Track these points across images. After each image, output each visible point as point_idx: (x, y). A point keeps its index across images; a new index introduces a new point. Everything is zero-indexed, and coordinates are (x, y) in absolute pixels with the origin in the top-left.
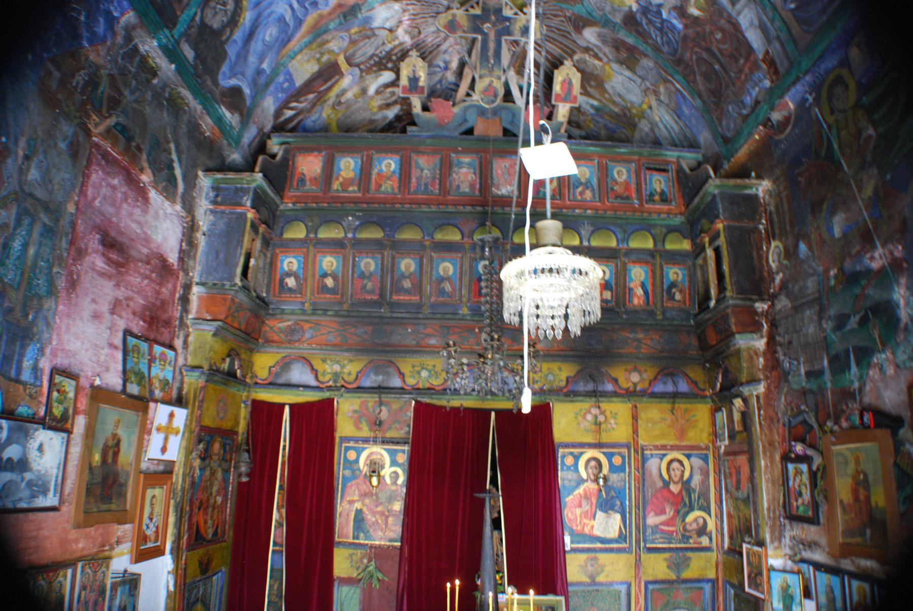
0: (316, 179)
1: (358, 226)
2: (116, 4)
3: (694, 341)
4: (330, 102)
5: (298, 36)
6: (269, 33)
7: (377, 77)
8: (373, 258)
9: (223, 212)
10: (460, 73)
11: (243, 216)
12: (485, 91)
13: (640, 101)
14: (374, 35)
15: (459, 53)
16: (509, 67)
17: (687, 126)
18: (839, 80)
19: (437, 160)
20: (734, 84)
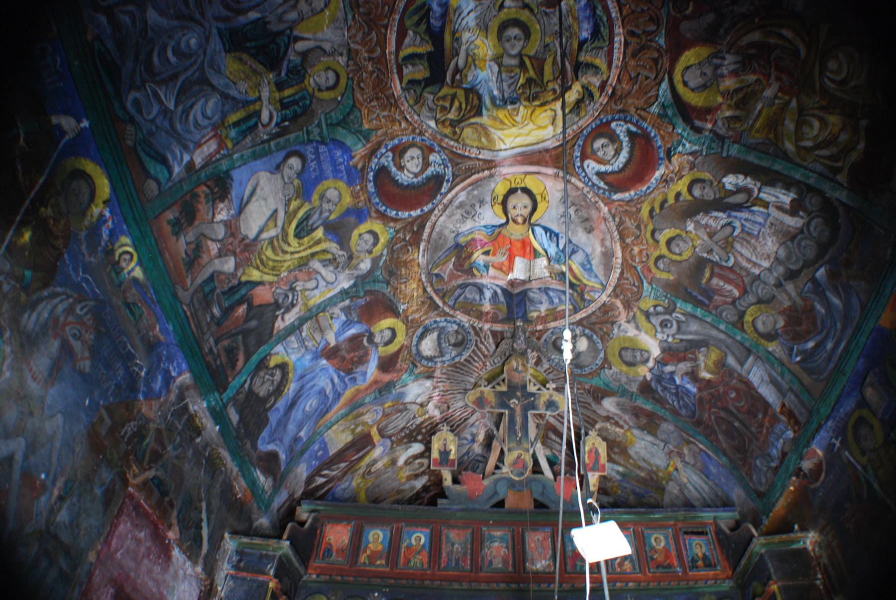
0: (343, 550)
2: (175, 364)
4: (361, 471)
5: (336, 408)
6: (310, 404)
7: (407, 449)
9: (244, 579)
10: (488, 444)
11: (264, 585)
12: (514, 464)
13: (665, 465)
14: (406, 409)
15: (486, 426)
16: (536, 439)
17: (717, 485)
18: (861, 420)
19: (468, 533)
20: (757, 439)
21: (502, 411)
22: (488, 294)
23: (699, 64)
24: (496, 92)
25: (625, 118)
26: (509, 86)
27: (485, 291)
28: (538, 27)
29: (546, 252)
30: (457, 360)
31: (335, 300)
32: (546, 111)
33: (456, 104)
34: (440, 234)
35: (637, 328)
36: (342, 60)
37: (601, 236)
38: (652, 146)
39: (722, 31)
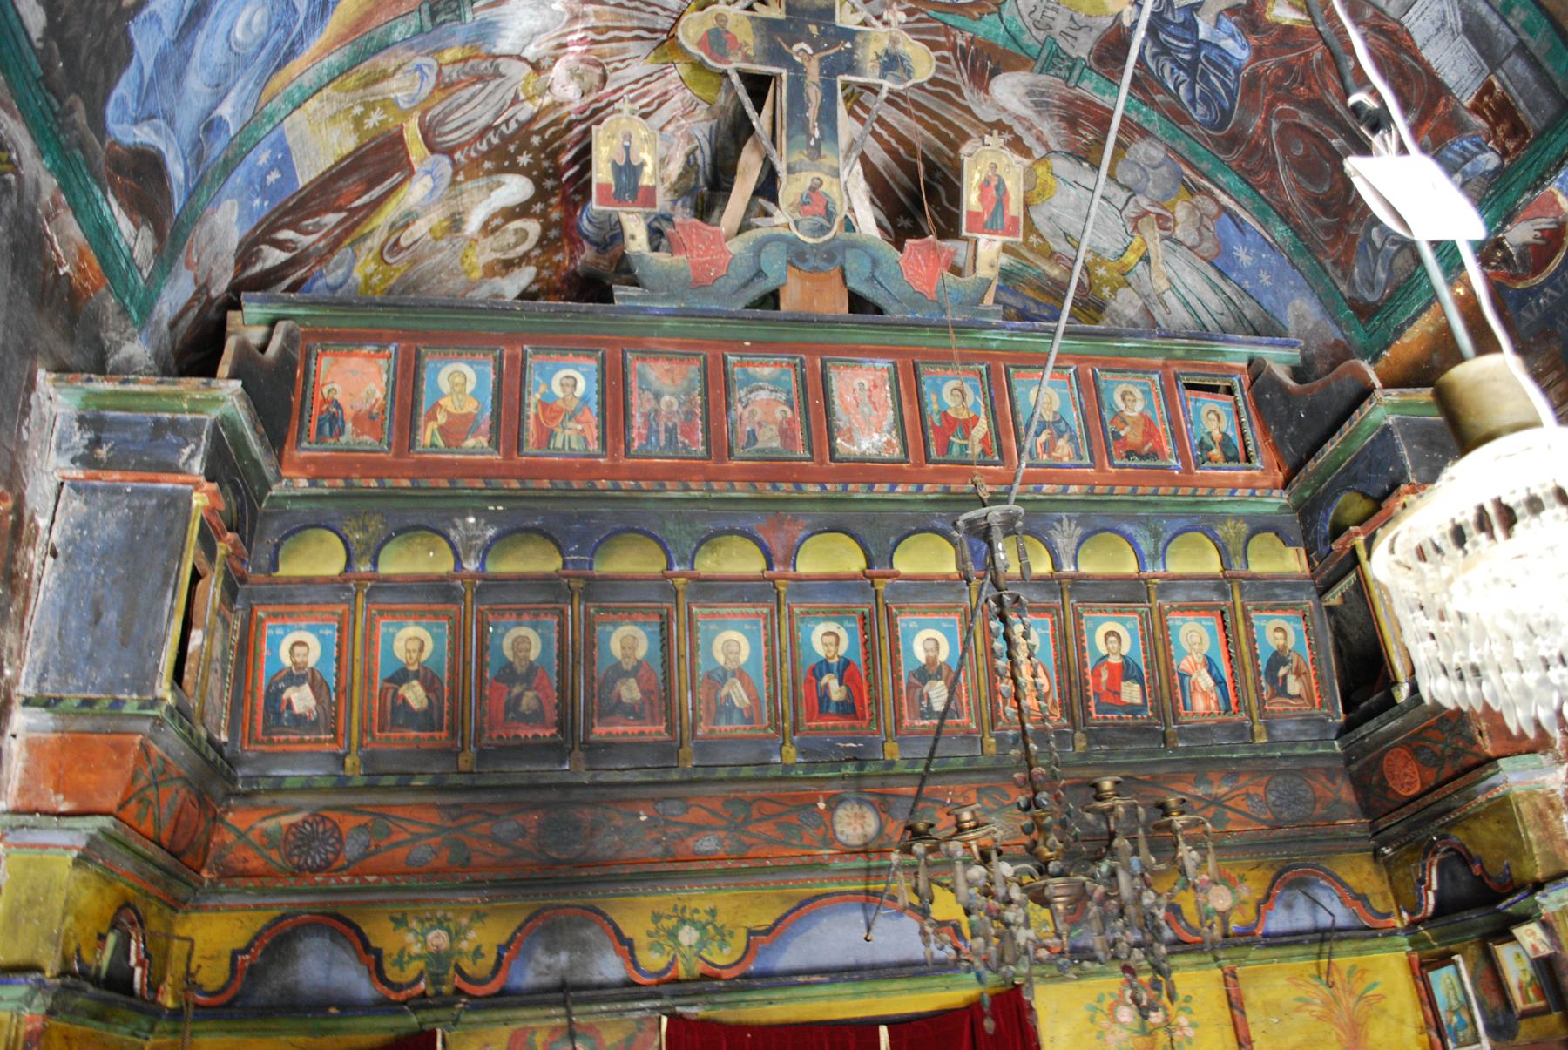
0: (370, 416)
1: (494, 540)
3: (1345, 792)
4: (375, 242)
8: (535, 627)
9: (114, 491)
11: (177, 503)
12: (803, 204)
14: (497, 74)
15: (690, 139)
19: (693, 371)
21: (774, 70)
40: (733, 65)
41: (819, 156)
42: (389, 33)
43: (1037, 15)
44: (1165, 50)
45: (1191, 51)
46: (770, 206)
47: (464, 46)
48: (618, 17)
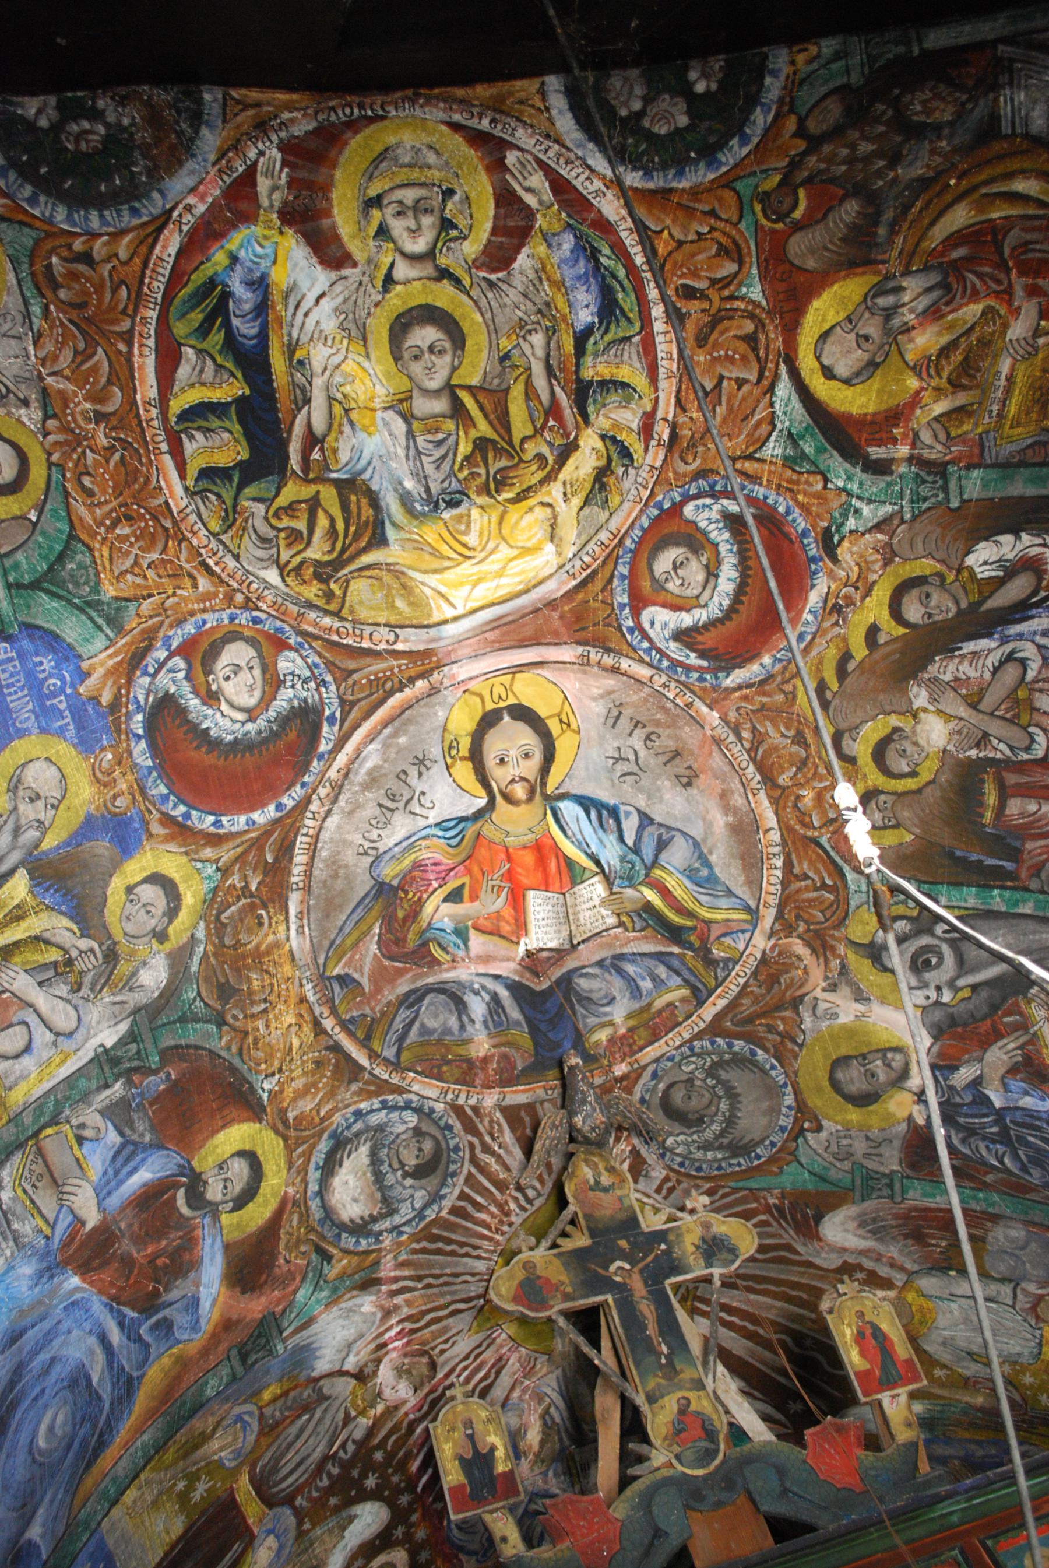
12: (678, 1431)
14: (323, 1398)
15: (539, 1397)
21: (599, 1298)
22: (478, 1007)
23: (849, 319)
24: (409, 484)
25: (712, 487)
26: (438, 464)
27: (470, 999)
28: (478, 318)
29: (598, 863)
30: (431, 1214)
31: (83, 1083)
32: (531, 509)
33: (323, 522)
34: (334, 863)
35: (859, 996)
36: (31, 416)
37: (718, 786)
38: (787, 536)
39: (882, 231)
40: (555, 1309)
41: (677, 1373)
42: (201, 1391)
43: (834, 1148)
44: (970, 1132)
45: (996, 1122)
46: (643, 1448)
47: (280, 1380)
48: (429, 1298)
